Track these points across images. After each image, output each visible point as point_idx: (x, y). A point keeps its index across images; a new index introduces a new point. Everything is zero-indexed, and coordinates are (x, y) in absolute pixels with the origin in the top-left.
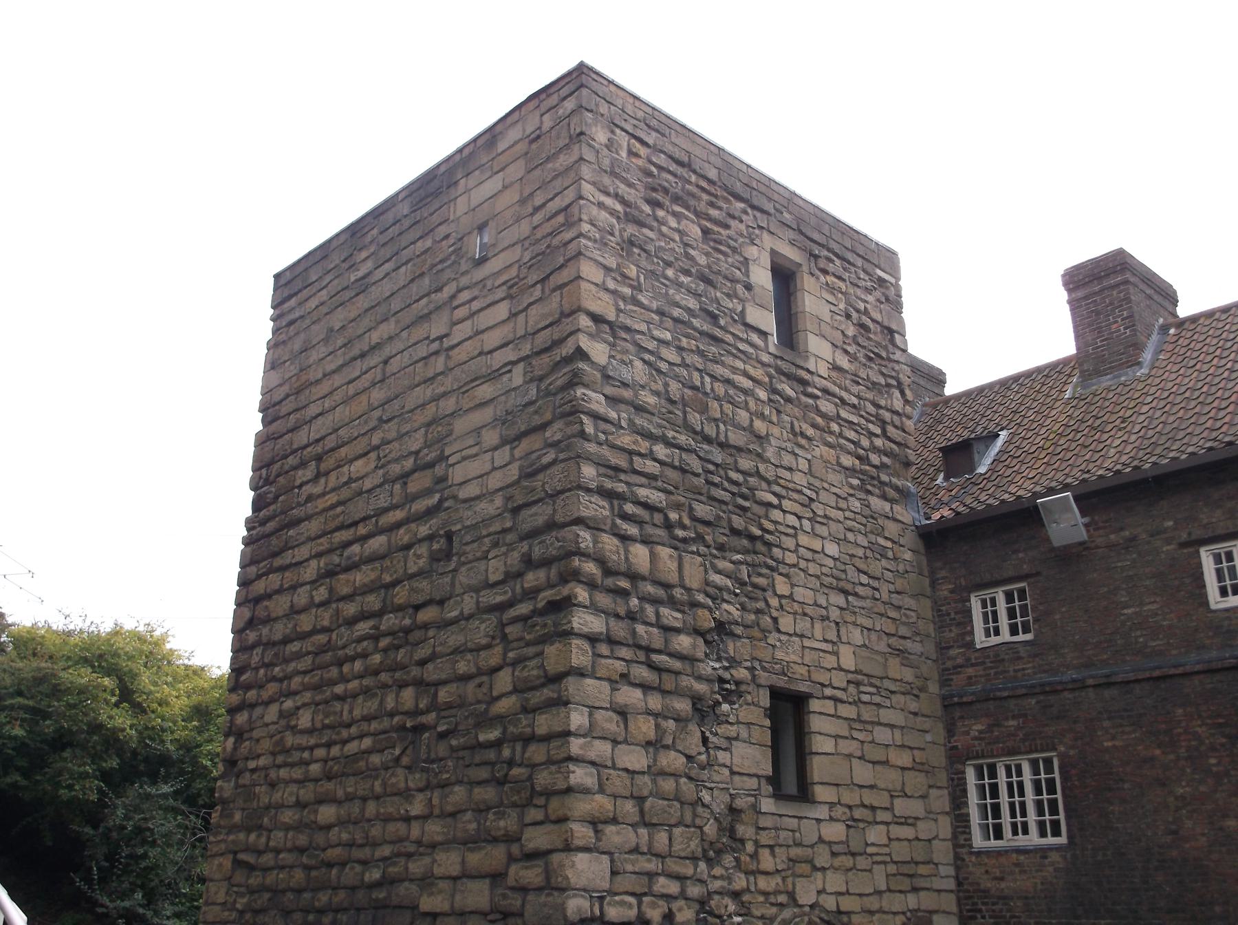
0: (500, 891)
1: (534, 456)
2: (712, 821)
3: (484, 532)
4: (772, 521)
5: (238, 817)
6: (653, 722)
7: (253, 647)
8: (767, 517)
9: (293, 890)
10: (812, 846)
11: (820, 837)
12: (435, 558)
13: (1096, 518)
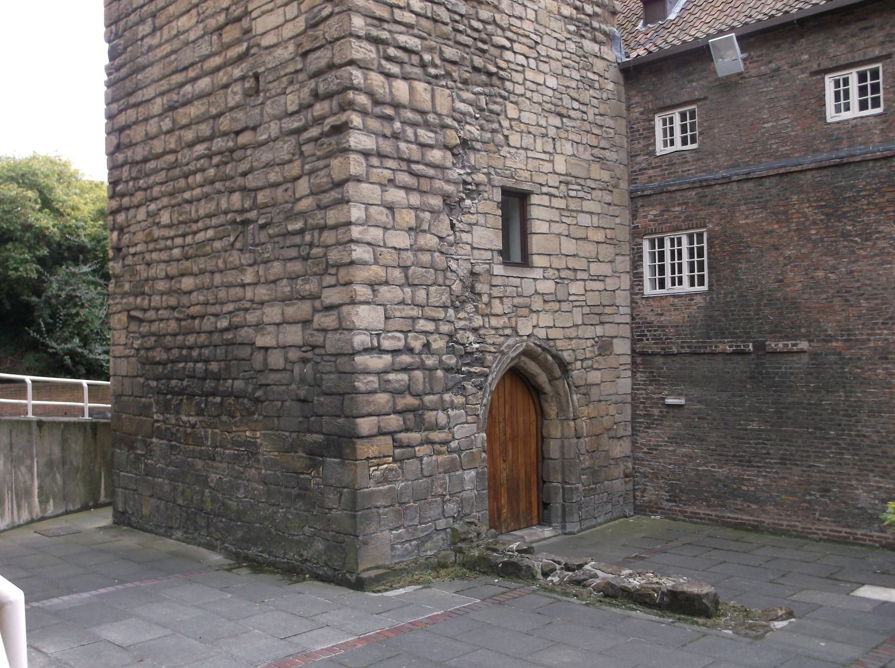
0: (309, 332)
1: (316, 10)
2: (458, 281)
3: (282, 73)
4: (505, 61)
5: (127, 287)
6: (414, 214)
7: (122, 166)
8: (501, 57)
9: (170, 335)
10: (530, 297)
11: (536, 290)
12: (247, 94)
13: (752, 53)
